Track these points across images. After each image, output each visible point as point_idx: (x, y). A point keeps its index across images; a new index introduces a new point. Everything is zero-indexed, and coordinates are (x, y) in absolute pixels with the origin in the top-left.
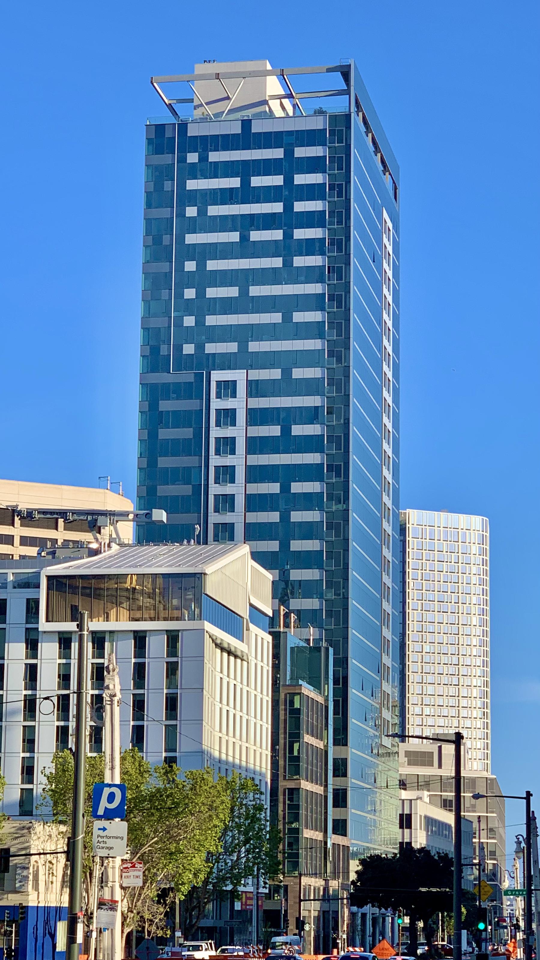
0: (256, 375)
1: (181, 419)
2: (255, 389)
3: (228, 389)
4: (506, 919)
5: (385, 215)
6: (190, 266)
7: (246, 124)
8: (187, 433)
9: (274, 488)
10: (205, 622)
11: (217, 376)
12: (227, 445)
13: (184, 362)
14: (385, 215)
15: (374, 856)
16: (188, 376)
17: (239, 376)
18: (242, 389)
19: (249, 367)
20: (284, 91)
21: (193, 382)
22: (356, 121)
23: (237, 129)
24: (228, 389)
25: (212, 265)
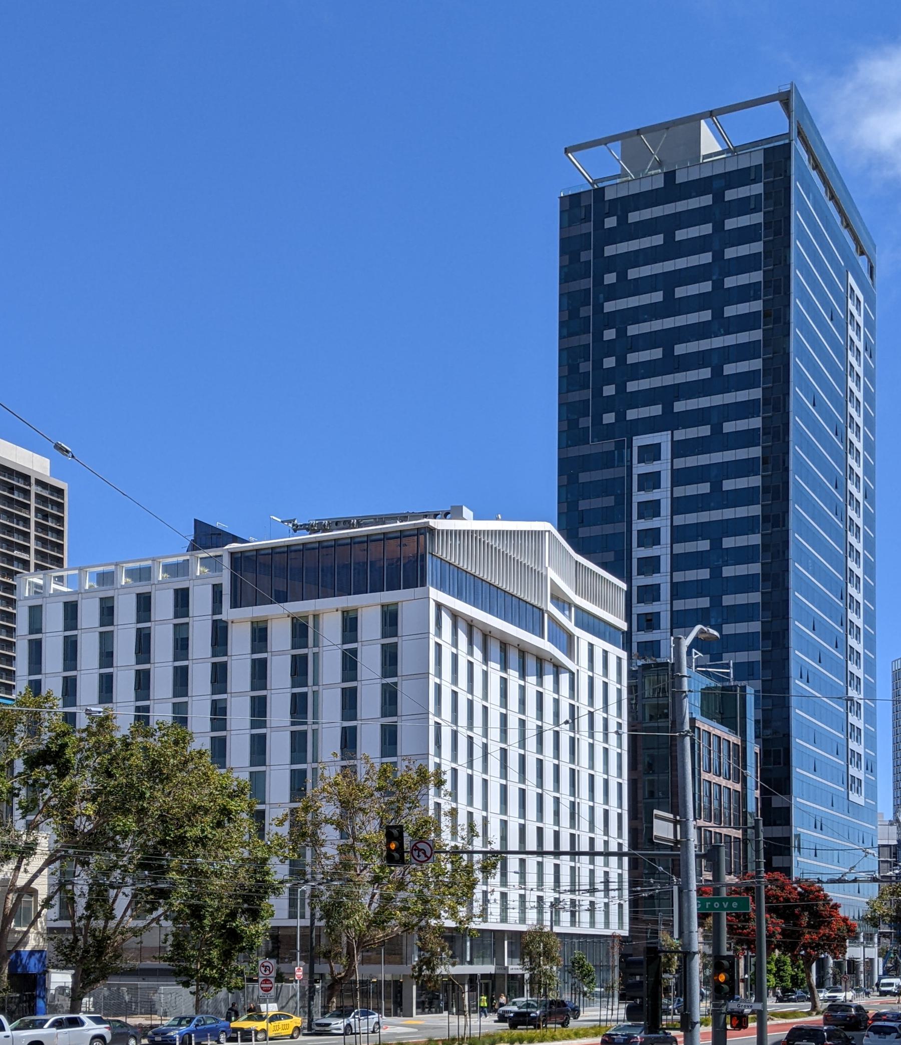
0: (681, 435)
1: (605, 487)
2: (680, 449)
3: (651, 453)
4: (673, 1033)
5: (851, 280)
6: (610, 334)
7: (670, 176)
8: (609, 501)
9: (704, 545)
10: (431, 588)
11: (640, 441)
12: (651, 509)
13: (607, 432)
14: (851, 280)
15: (817, 898)
16: (609, 445)
17: (663, 439)
18: (666, 451)
19: (672, 428)
20: (721, 146)
21: (613, 451)
22: (797, 146)
23: (660, 183)
24: (651, 453)
25: (633, 330)
